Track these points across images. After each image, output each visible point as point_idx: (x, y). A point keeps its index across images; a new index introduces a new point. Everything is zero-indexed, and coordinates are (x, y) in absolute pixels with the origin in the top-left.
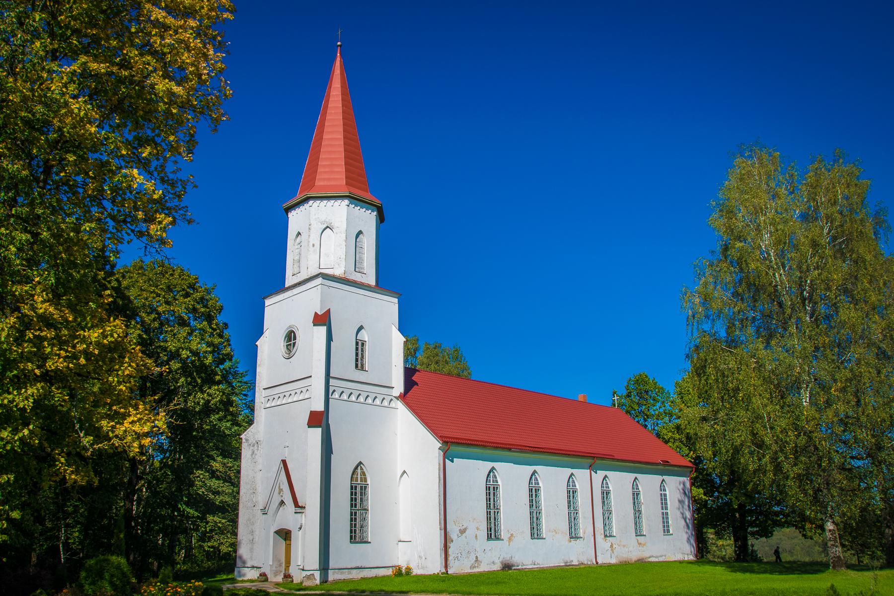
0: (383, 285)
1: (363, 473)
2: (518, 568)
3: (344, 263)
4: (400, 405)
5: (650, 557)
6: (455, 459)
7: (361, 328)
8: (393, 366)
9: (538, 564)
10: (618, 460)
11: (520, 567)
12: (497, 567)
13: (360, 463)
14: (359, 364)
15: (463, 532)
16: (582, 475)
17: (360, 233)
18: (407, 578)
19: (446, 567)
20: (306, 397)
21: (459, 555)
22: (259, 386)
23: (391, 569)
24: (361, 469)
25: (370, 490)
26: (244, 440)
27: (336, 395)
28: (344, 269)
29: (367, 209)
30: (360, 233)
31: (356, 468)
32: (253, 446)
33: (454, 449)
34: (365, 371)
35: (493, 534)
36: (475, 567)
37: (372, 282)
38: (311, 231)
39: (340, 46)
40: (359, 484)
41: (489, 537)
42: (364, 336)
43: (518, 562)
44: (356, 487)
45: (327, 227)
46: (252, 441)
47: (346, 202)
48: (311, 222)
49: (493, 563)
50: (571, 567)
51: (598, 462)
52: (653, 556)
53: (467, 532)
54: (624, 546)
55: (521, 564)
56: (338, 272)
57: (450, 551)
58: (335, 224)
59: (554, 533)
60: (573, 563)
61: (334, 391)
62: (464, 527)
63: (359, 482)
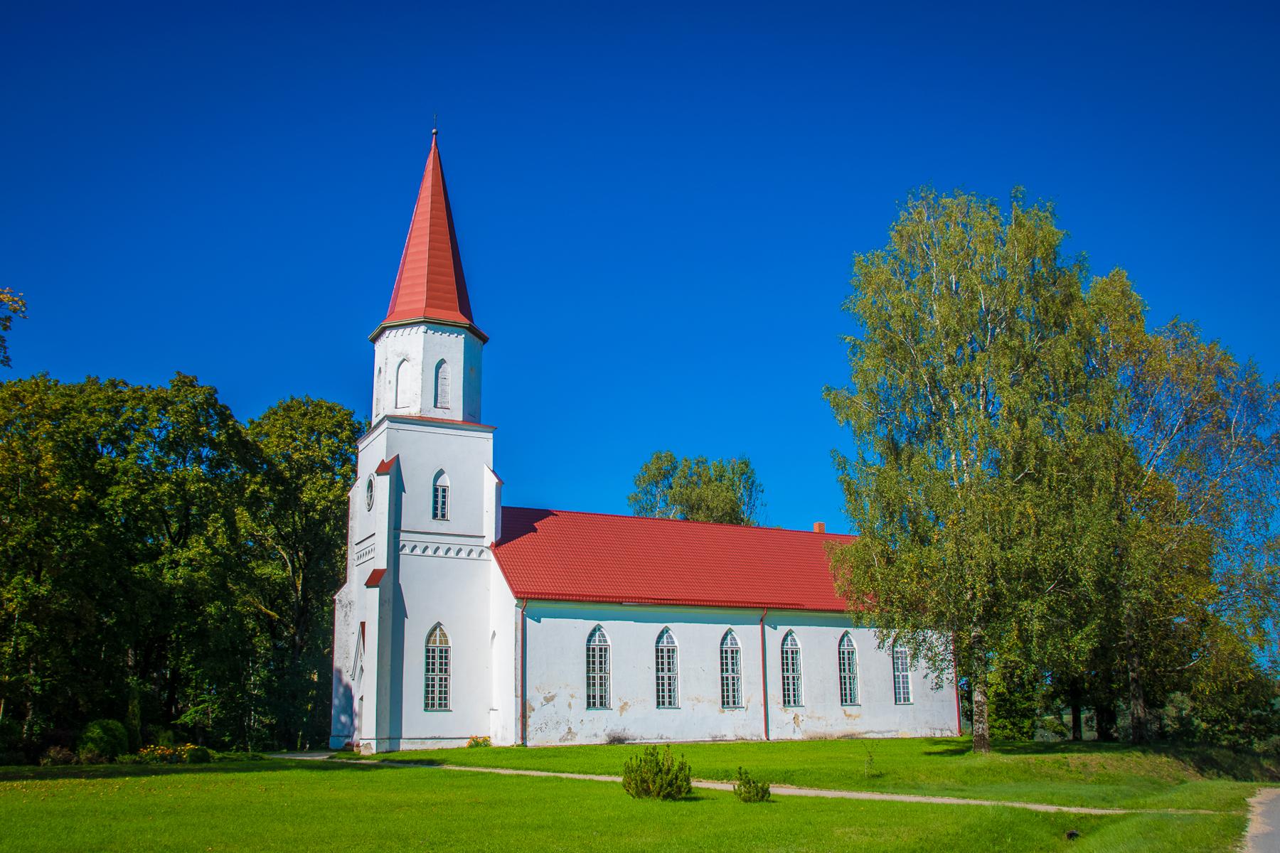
0: (473, 418)
1: (444, 635)
2: (634, 742)
3: (420, 400)
4: (489, 555)
5: (866, 733)
6: (542, 619)
7: (440, 473)
8: (485, 512)
9: (667, 738)
10: (809, 610)
11: (637, 741)
12: (603, 739)
13: (439, 624)
14: (439, 511)
15: (549, 700)
16: (746, 635)
17: (442, 362)
18: (483, 749)
19: (524, 738)
20: (372, 556)
21: (544, 725)
22: (351, 542)
23: (466, 740)
24: (441, 630)
25: (452, 655)
26: (337, 601)
27: (407, 550)
28: (419, 407)
29: (452, 333)
30: (442, 362)
31: (434, 629)
32: (346, 607)
33: (535, 606)
34: (447, 520)
35: (597, 699)
36: (567, 740)
37: (458, 415)
38: (388, 366)
39: (436, 133)
40: (437, 647)
41: (590, 704)
42: (445, 481)
43: (635, 735)
44: (434, 651)
45: (404, 360)
46: (345, 601)
47: (423, 328)
48: (389, 356)
49: (596, 735)
50: (724, 742)
51: (771, 613)
52: (872, 732)
53: (556, 699)
54: (819, 718)
55: (639, 737)
56: (414, 411)
57: (530, 721)
58: (411, 356)
59: (695, 702)
60: (725, 738)
61: (404, 546)
62: (550, 694)
63: (438, 645)
